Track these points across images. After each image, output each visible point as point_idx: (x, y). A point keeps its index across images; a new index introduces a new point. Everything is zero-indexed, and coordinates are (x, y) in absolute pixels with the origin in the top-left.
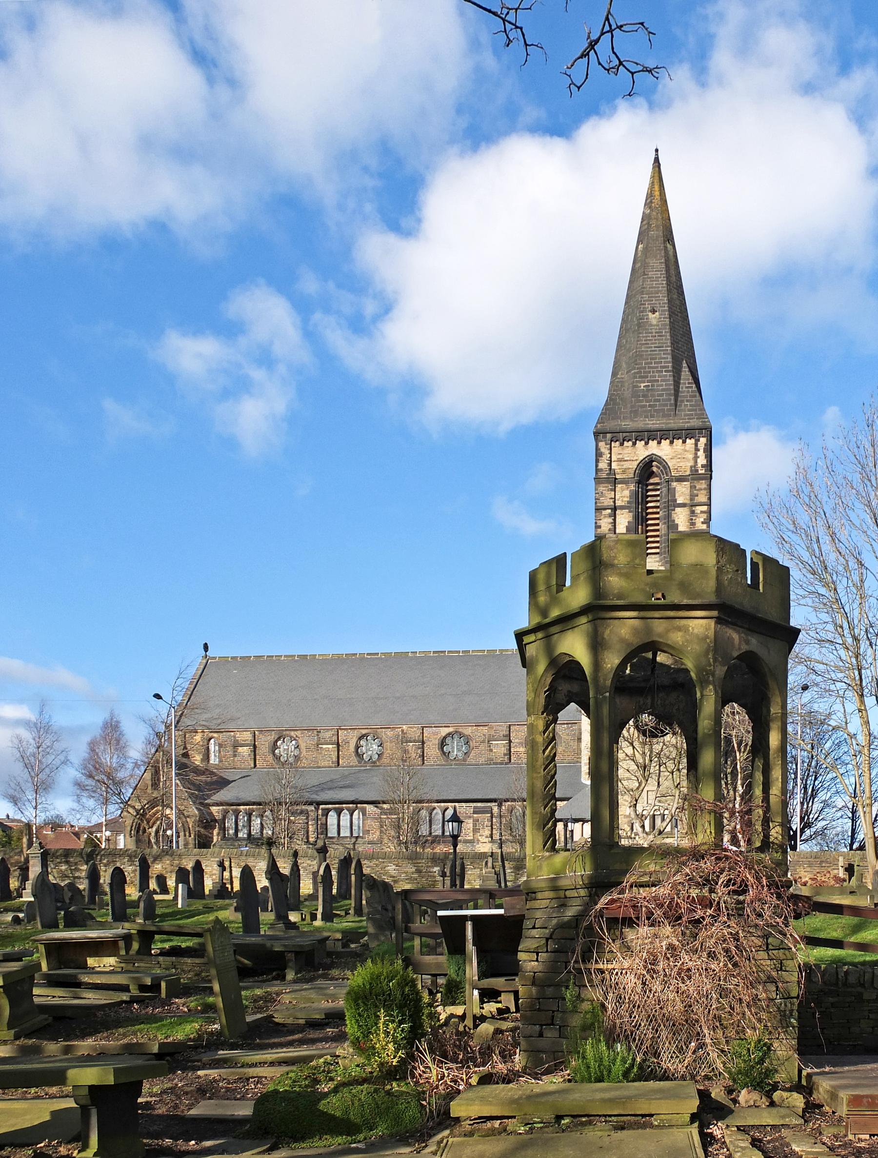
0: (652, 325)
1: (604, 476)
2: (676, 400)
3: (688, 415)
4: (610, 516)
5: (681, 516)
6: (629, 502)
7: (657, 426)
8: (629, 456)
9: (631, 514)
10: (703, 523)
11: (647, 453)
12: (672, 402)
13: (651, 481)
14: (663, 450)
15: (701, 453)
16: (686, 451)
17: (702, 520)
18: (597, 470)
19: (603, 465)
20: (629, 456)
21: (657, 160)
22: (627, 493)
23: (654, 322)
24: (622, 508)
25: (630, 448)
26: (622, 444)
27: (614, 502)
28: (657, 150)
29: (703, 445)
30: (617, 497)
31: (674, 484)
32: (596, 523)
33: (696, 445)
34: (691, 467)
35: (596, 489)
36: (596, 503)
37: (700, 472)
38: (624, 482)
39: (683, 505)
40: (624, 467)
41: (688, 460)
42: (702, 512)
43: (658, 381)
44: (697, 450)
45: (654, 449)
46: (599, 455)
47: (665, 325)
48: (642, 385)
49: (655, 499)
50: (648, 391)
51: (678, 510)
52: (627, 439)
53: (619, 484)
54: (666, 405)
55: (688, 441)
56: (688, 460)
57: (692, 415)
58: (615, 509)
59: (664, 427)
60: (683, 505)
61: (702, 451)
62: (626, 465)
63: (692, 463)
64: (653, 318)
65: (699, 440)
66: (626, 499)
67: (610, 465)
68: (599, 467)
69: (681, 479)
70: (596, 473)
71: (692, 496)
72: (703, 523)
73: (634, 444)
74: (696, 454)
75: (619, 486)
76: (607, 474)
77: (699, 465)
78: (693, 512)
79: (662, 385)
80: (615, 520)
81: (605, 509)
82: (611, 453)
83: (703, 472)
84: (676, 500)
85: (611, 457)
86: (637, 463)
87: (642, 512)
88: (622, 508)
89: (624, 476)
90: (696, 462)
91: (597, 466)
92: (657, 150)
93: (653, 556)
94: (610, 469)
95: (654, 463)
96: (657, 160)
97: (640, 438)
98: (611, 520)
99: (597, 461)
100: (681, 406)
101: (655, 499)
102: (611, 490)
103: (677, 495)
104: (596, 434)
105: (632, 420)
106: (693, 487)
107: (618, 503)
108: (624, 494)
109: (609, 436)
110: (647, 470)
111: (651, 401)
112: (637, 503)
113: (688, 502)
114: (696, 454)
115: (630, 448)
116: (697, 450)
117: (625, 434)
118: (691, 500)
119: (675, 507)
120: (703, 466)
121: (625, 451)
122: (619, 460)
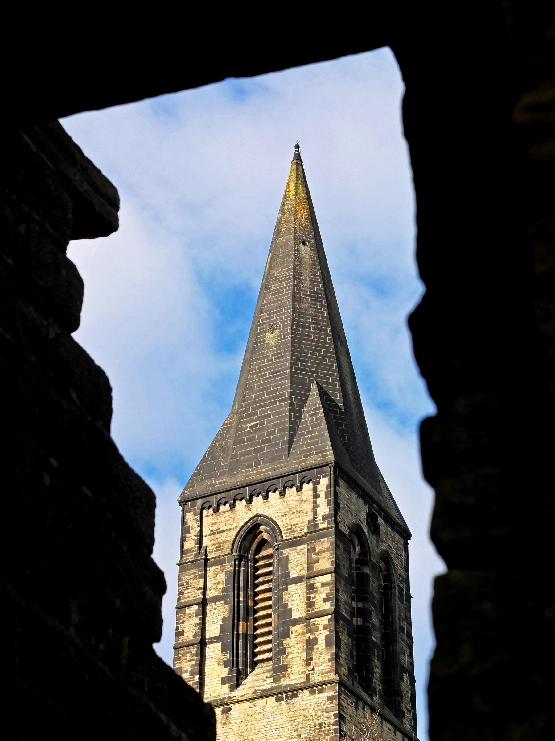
0: (268, 347)
1: (191, 558)
2: (291, 436)
3: (305, 451)
4: (196, 615)
5: (296, 596)
6: (224, 590)
7: (261, 476)
8: (230, 521)
9: (227, 607)
10: (325, 600)
11: (250, 515)
12: (286, 439)
13: (263, 553)
14: (271, 507)
15: (322, 501)
16: (302, 501)
17: (324, 596)
18: (183, 552)
19: (191, 544)
20: (230, 521)
21: (298, 157)
22: (222, 577)
23: (272, 343)
24: (215, 599)
25: (227, 514)
26: (217, 510)
27: (204, 593)
28: (297, 147)
29: (324, 488)
30: (209, 586)
31: (286, 551)
32: (177, 628)
33: (315, 490)
34: (309, 522)
35: (180, 580)
36: (179, 599)
37: (321, 526)
38: (219, 561)
39: (299, 579)
40: (219, 541)
41: (306, 513)
42: (323, 585)
43: (269, 416)
44: (316, 496)
45: (259, 506)
46: (185, 529)
47: (286, 343)
48: (249, 426)
49: (267, 578)
50: (255, 431)
51: (292, 588)
52: (223, 501)
53: (212, 565)
54: (277, 445)
55: (305, 486)
56: (306, 513)
57: (310, 450)
58: (204, 603)
59: (271, 474)
60: (299, 579)
61: (323, 496)
62: (221, 537)
63: (310, 517)
64: (271, 338)
65: (318, 483)
66: (221, 586)
67: (200, 542)
68: (185, 548)
69: (294, 543)
70: (182, 557)
71: (311, 564)
72: (325, 600)
73: (233, 506)
74: (315, 503)
75: (212, 569)
76: (196, 555)
77: (320, 517)
78: (310, 587)
79: (274, 420)
80: (203, 620)
81: (190, 606)
82: (201, 526)
83: (325, 525)
84: (288, 574)
85: (201, 531)
86: (235, 532)
87: (246, 602)
88: (215, 599)
89: (219, 553)
90: (315, 513)
91: (182, 546)
92: (297, 147)
93: (265, 664)
94: (200, 547)
95: (262, 528)
96: (298, 157)
97: (239, 497)
98: (197, 620)
99: (183, 540)
100: (298, 441)
101: (267, 578)
102: (200, 577)
103: (290, 566)
104: (183, 502)
105: (231, 475)
106: (311, 551)
107: (210, 594)
108: (218, 580)
109: (199, 502)
110: (252, 539)
111: (258, 444)
112: (237, 588)
113: (305, 573)
114: (315, 503)
115: (227, 514)
116: (316, 496)
117: (219, 496)
118: (309, 569)
119: (287, 584)
120: (324, 518)
121: (222, 519)
122: (213, 533)
